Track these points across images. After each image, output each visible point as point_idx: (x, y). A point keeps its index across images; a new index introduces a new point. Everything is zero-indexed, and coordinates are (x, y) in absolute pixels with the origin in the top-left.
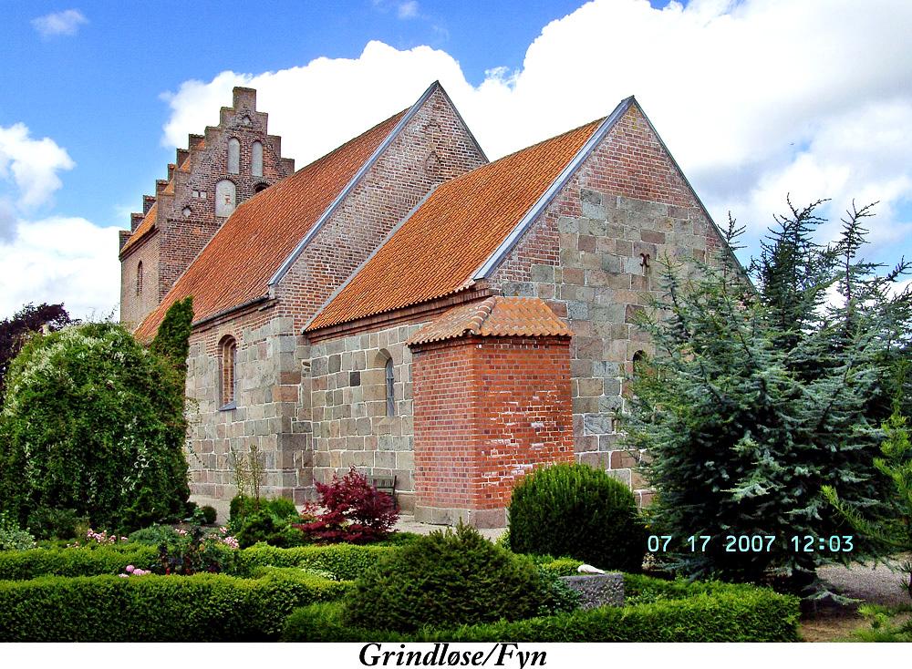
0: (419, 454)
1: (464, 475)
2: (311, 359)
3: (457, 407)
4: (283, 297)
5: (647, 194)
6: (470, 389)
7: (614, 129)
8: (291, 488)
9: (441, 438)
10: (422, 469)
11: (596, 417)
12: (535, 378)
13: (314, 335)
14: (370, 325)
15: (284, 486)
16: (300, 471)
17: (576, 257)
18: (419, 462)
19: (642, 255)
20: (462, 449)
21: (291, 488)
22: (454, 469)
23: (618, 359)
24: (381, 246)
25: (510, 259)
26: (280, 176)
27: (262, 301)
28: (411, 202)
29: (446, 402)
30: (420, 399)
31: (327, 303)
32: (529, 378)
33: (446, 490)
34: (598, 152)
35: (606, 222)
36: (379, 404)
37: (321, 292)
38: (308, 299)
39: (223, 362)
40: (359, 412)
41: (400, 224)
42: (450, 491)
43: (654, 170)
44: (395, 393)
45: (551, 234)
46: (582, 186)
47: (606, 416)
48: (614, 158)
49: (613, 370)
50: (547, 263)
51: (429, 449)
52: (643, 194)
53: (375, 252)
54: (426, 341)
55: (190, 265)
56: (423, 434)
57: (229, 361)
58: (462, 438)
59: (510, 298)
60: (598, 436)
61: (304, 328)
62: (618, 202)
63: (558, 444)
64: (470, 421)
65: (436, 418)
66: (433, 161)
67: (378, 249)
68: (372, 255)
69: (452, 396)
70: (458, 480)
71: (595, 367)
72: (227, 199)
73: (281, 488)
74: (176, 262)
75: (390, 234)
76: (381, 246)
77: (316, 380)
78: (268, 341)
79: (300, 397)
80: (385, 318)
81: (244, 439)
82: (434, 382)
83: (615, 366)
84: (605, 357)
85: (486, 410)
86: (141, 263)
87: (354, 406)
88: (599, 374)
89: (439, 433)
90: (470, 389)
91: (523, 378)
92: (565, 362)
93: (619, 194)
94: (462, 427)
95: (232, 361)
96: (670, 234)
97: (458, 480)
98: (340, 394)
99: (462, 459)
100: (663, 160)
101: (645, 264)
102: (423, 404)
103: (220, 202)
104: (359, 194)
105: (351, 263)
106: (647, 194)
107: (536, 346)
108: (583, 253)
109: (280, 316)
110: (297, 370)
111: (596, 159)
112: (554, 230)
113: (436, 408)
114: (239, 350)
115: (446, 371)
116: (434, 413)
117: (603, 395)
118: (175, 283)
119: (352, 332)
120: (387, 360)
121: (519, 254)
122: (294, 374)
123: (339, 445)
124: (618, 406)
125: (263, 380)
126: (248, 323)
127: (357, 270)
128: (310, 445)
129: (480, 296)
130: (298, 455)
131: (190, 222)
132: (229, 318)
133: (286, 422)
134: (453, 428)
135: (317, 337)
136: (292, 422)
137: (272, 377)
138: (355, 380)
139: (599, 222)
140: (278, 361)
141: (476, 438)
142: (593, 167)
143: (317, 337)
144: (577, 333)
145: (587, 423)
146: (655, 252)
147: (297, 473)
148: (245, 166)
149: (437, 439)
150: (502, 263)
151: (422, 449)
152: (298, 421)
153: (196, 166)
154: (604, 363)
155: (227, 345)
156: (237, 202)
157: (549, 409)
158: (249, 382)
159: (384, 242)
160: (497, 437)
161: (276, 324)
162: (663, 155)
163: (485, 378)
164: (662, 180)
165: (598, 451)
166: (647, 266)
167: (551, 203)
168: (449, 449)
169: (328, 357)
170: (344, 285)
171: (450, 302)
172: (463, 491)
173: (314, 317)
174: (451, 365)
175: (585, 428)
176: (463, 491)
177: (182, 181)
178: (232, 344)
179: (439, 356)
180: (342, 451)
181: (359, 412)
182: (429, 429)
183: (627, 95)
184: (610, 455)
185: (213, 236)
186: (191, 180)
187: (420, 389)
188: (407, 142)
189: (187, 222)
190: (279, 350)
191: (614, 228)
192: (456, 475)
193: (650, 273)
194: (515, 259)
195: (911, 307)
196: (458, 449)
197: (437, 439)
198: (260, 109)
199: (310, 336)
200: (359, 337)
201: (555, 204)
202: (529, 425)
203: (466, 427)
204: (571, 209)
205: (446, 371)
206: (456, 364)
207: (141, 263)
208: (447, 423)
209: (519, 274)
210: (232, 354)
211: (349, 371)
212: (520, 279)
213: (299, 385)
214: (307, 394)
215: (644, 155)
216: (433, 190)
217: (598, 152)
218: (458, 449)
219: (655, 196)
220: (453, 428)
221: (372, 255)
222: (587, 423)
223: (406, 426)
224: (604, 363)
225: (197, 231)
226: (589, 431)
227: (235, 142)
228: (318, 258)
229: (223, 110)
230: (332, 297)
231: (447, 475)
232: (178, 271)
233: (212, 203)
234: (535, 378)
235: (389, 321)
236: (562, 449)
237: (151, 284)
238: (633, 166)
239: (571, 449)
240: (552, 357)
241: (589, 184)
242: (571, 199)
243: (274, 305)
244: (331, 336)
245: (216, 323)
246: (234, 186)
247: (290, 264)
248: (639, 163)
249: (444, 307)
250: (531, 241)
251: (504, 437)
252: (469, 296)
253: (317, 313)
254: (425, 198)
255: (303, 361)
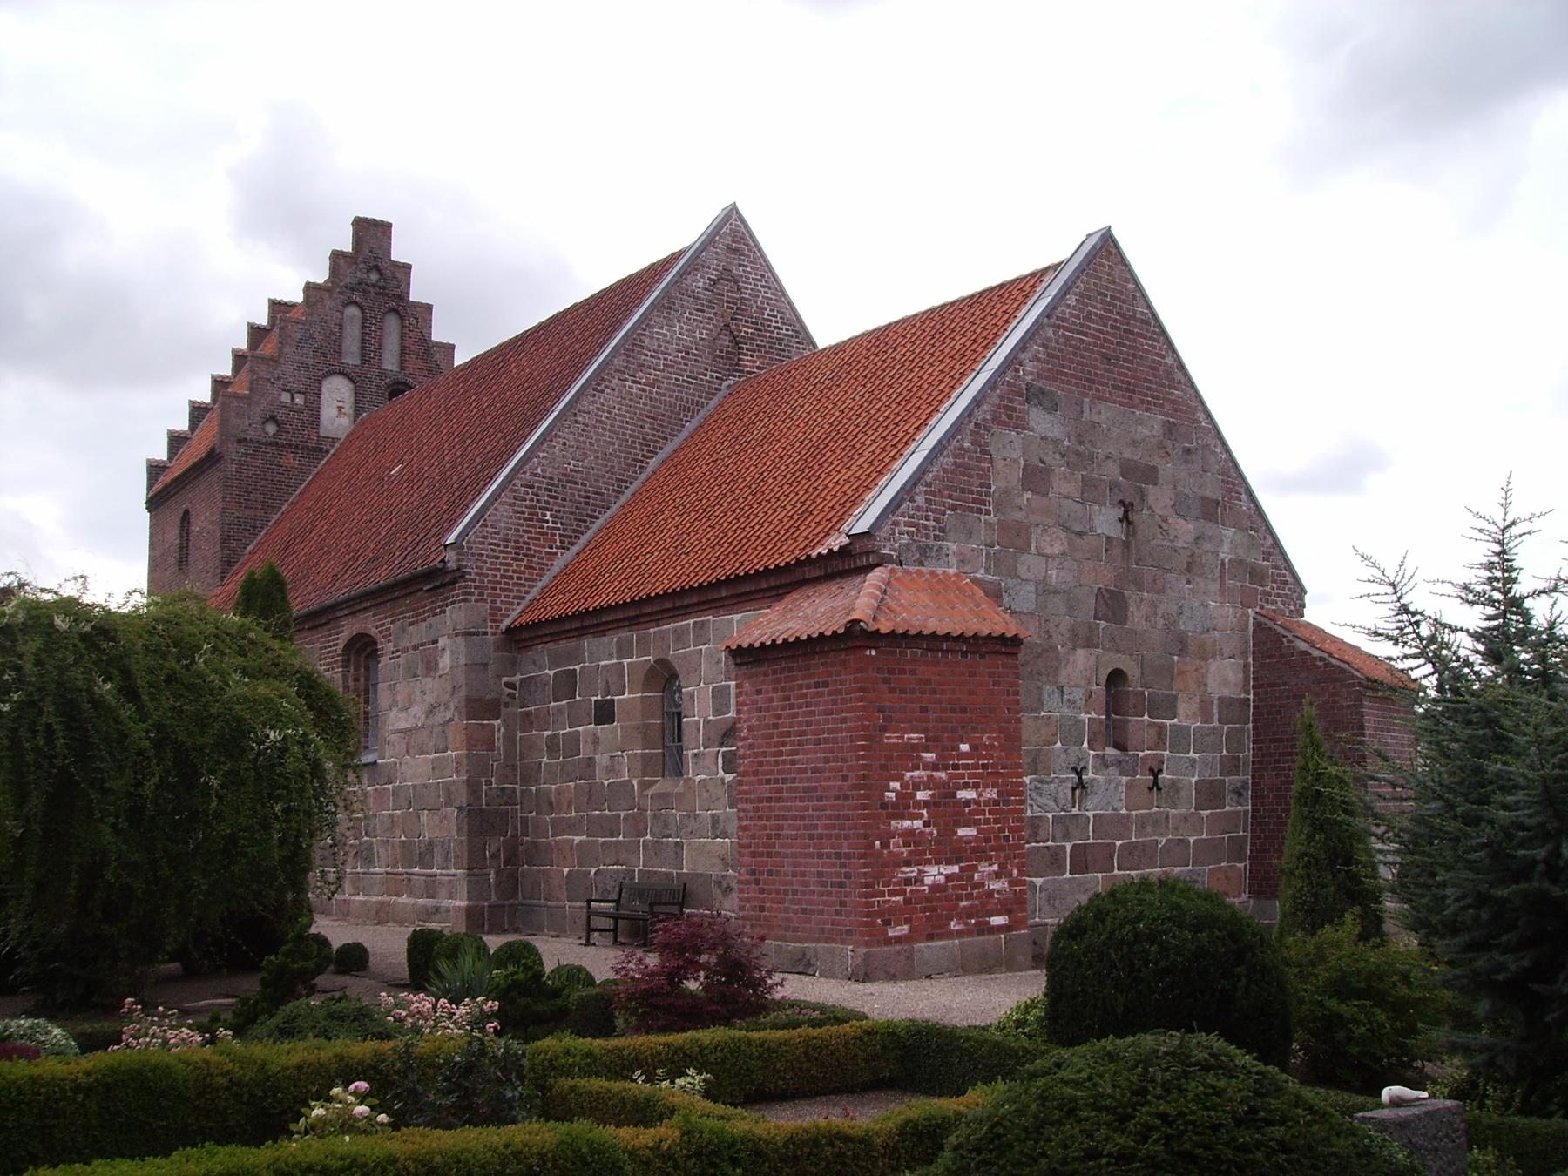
0: (749, 846)
1: (841, 885)
2: (519, 677)
3: (827, 760)
4: (472, 569)
5: (1130, 398)
6: (856, 729)
7: (1079, 283)
8: (481, 903)
9: (794, 818)
10: (753, 873)
11: (1047, 783)
12: (964, 711)
13: (525, 635)
14: (637, 617)
15: (469, 899)
16: (497, 873)
17: (1018, 501)
18: (747, 859)
19: (1122, 502)
20: (838, 837)
21: (481, 903)
22: (820, 874)
23: (1083, 683)
24: (637, 484)
25: (912, 501)
26: (430, 371)
27: (431, 574)
28: (691, 408)
29: (805, 752)
30: (751, 746)
31: (546, 579)
32: (953, 711)
33: (804, 911)
34: (1053, 320)
35: (1066, 443)
36: (651, 756)
37: (535, 560)
38: (514, 571)
39: (351, 683)
40: (611, 770)
41: (670, 448)
42: (812, 912)
43: (1141, 357)
44: (685, 738)
45: (979, 460)
46: (1028, 378)
47: (1063, 781)
48: (1078, 332)
49: (1074, 702)
50: (971, 510)
51: (769, 837)
52: (1124, 396)
53: (628, 493)
54: (769, 643)
55: (276, 517)
56: (756, 809)
57: (362, 680)
58: (838, 817)
59: (912, 569)
60: (1050, 815)
61: (507, 622)
62: (1086, 408)
63: (1001, 830)
64: (854, 787)
65: (784, 781)
66: (725, 341)
67: (632, 488)
68: (623, 499)
69: (818, 742)
70: (829, 894)
71: (1046, 696)
72: (339, 407)
73: (464, 903)
74: (252, 512)
75: (653, 463)
76: (637, 484)
77: (528, 714)
78: (441, 643)
79: (499, 743)
80: (668, 605)
81: (391, 816)
82: (779, 717)
83: (1078, 694)
84: (1062, 680)
85: (883, 767)
86: (186, 512)
87: (602, 759)
88: (1054, 708)
89: (789, 809)
90: (856, 729)
91: (943, 710)
92: (1011, 684)
93: (1086, 395)
94: (837, 798)
95: (367, 680)
96: (1166, 469)
97: (829, 894)
98: (575, 738)
99: (838, 856)
100: (1155, 340)
101: (1125, 519)
102: (756, 755)
103: (328, 412)
104: (602, 391)
105: (587, 508)
106: (1130, 398)
107: (964, 654)
108: (1028, 495)
109: (465, 600)
110: (494, 695)
111: (1050, 333)
112: (984, 452)
113: (784, 762)
114: (384, 661)
115: (805, 695)
116: (780, 772)
117: (1059, 744)
118: (250, 548)
119: (600, 630)
120: (664, 677)
121: (926, 493)
122: (489, 700)
123: (573, 827)
124: (1082, 764)
125: (431, 711)
126: (401, 613)
127: (599, 523)
128: (515, 828)
129: (859, 563)
130: (494, 845)
131: (277, 444)
132: (365, 605)
133: (473, 787)
134: (820, 799)
135: (531, 639)
136: (484, 787)
137: (447, 708)
138: (605, 713)
139: (1056, 442)
140: (462, 678)
141: (865, 817)
142: (1043, 346)
143: (531, 639)
144: (1030, 632)
145: (1034, 795)
146: (1142, 499)
147: (492, 877)
148: (370, 349)
149: (785, 818)
150: (899, 506)
151: (753, 837)
152: (494, 785)
153: (288, 349)
154: (1061, 689)
155: (358, 652)
156: (357, 413)
157: (984, 767)
158: (403, 715)
159: (643, 477)
160: (902, 817)
161: (456, 615)
162: (1154, 333)
163: (881, 710)
164: (1154, 375)
165: (1050, 843)
166: (1129, 523)
167: (978, 406)
168: (811, 837)
169: (551, 673)
170: (575, 549)
171: (798, 575)
172: (838, 913)
173: (524, 603)
174: (816, 685)
175: (1029, 802)
176: (838, 913)
177: (262, 374)
178: (369, 650)
179: (791, 670)
180: (577, 839)
181: (611, 770)
182: (769, 800)
183: (1097, 225)
184: (1068, 850)
185: (316, 470)
186: (278, 373)
187: (750, 728)
188: (682, 306)
189: (271, 444)
190: (463, 661)
191: (1078, 454)
192: (824, 884)
193: (1134, 534)
194: (920, 500)
195: (1, 799)
196: (829, 837)
197: (785, 818)
198: (397, 256)
199: (520, 638)
200: (613, 639)
201: (985, 407)
202: (954, 795)
203: (846, 798)
204: (1010, 417)
205: (805, 695)
206: (826, 684)
207: (186, 512)
208: (805, 790)
209: (926, 527)
210: (367, 669)
211: (594, 698)
212: (927, 536)
213: (497, 723)
214: (509, 738)
215: (1125, 331)
216: (724, 392)
217: (1053, 320)
218: (829, 837)
219: (1142, 402)
220: (820, 799)
221: (623, 499)
222: (1034, 795)
223: (705, 795)
224: (1061, 689)
225: (290, 460)
226: (1035, 807)
227: (353, 311)
228: (532, 500)
229: (336, 257)
230: (556, 569)
231: (806, 884)
232: (255, 527)
233: (313, 410)
234: (964, 711)
235: (674, 609)
236: (1007, 838)
237: (206, 550)
238: (1108, 348)
239: (1021, 838)
240: (991, 675)
241: (1040, 376)
242: (1011, 401)
243: (455, 581)
244: (557, 637)
245: (339, 614)
246: (351, 386)
247: (484, 508)
248: (1118, 344)
249: (786, 585)
250: (945, 471)
251: (912, 817)
252: (838, 565)
253: (529, 597)
254: (713, 403)
255: (505, 679)
